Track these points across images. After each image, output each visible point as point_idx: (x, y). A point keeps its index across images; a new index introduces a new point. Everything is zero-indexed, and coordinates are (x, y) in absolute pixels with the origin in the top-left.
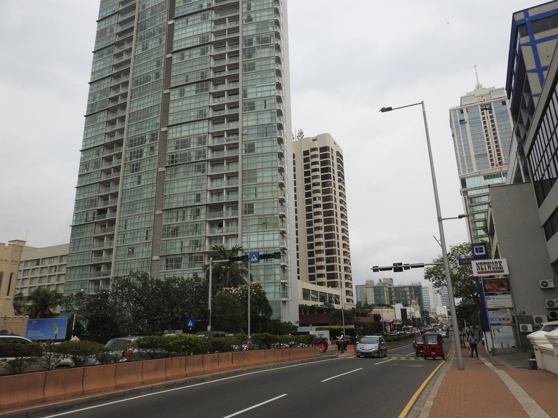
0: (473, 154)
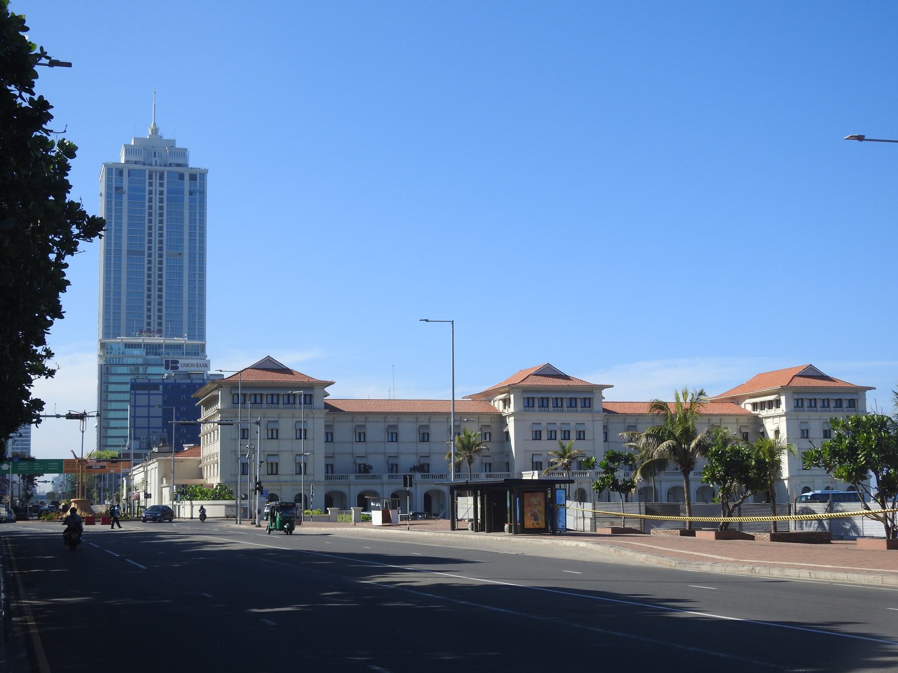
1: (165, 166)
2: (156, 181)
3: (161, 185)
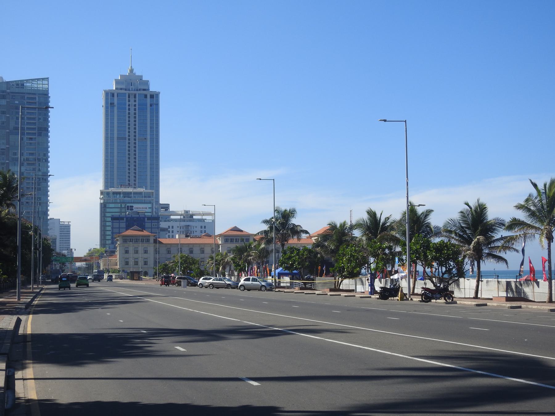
0: (116, 136)
1: (137, 90)
2: (132, 99)
3: (135, 101)
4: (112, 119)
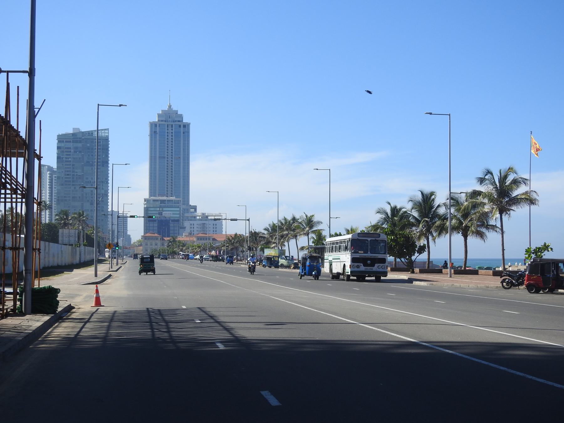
0: (158, 155)
2: (170, 128)
4: (155, 143)
